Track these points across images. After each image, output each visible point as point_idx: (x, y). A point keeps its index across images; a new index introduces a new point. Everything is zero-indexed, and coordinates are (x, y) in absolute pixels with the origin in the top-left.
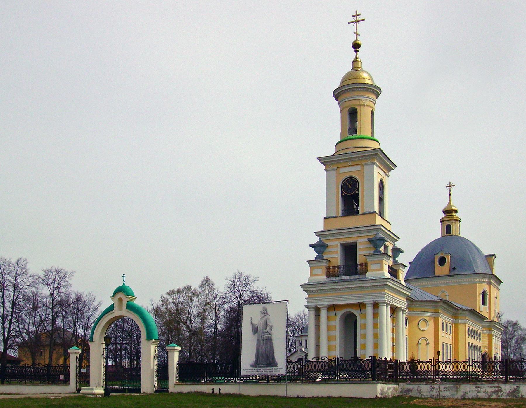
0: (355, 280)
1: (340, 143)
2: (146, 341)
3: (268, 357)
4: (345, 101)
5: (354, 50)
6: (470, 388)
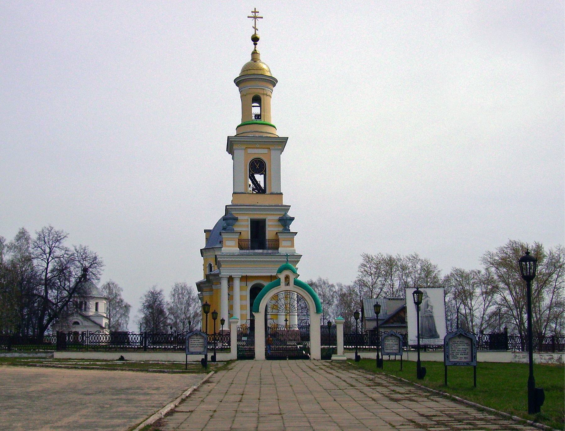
0: (267, 254)
1: (242, 127)
2: (316, 314)
3: (430, 330)
4: (250, 87)
5: (253, 42)
6: (537, 356)
